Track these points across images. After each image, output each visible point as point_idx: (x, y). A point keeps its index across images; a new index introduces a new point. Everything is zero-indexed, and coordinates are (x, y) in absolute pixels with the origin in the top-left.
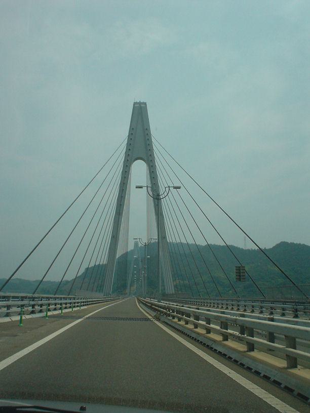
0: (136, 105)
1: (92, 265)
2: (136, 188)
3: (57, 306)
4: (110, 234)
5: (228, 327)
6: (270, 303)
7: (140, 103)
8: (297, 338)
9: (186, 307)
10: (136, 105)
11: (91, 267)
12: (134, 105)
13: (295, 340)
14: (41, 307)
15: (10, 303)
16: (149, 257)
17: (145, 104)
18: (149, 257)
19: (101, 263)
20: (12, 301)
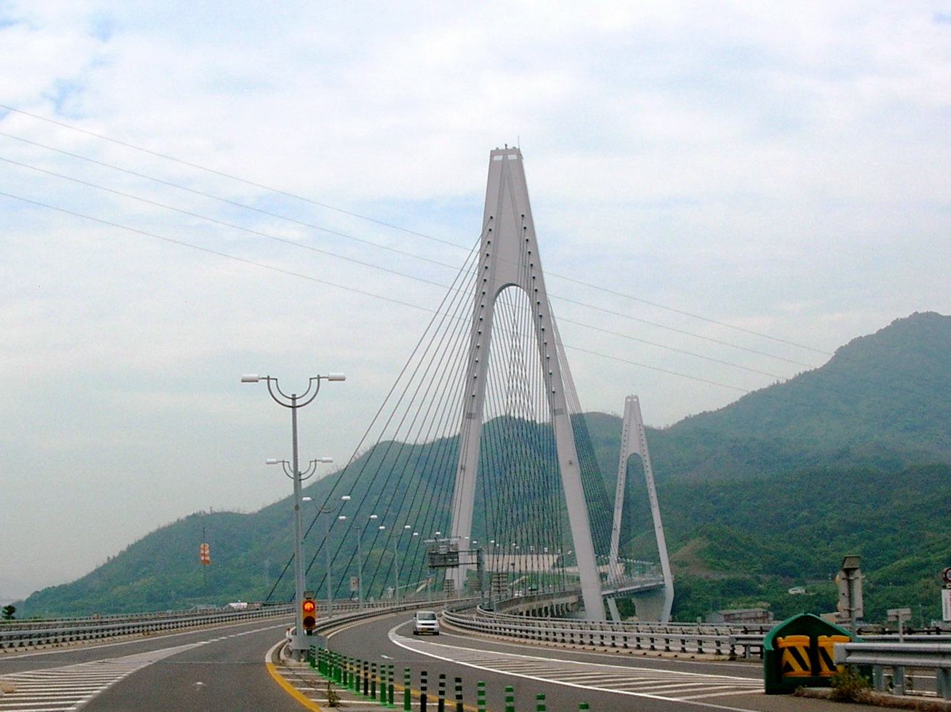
1: (431, 438)
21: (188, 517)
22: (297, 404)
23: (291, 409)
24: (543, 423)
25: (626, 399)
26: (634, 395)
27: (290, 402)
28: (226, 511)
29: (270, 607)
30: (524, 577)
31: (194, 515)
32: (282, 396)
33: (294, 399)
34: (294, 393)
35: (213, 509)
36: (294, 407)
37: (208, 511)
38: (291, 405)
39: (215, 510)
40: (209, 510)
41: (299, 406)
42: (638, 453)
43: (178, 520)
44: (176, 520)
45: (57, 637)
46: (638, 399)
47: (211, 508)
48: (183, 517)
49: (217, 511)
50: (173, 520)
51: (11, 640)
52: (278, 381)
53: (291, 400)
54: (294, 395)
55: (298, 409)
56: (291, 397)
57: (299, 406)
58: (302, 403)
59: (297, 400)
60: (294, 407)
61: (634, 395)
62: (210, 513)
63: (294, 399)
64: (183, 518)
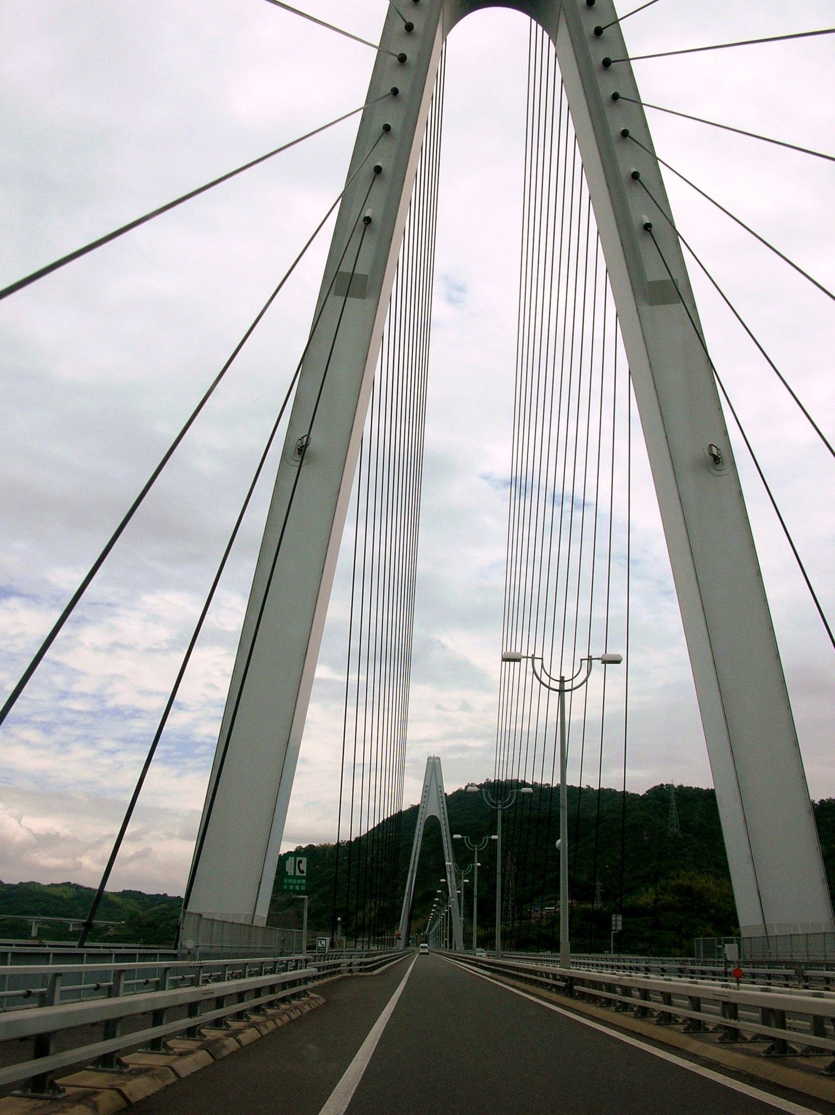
25: (428, 759)
42: (437, 816)
46: (440, 760)
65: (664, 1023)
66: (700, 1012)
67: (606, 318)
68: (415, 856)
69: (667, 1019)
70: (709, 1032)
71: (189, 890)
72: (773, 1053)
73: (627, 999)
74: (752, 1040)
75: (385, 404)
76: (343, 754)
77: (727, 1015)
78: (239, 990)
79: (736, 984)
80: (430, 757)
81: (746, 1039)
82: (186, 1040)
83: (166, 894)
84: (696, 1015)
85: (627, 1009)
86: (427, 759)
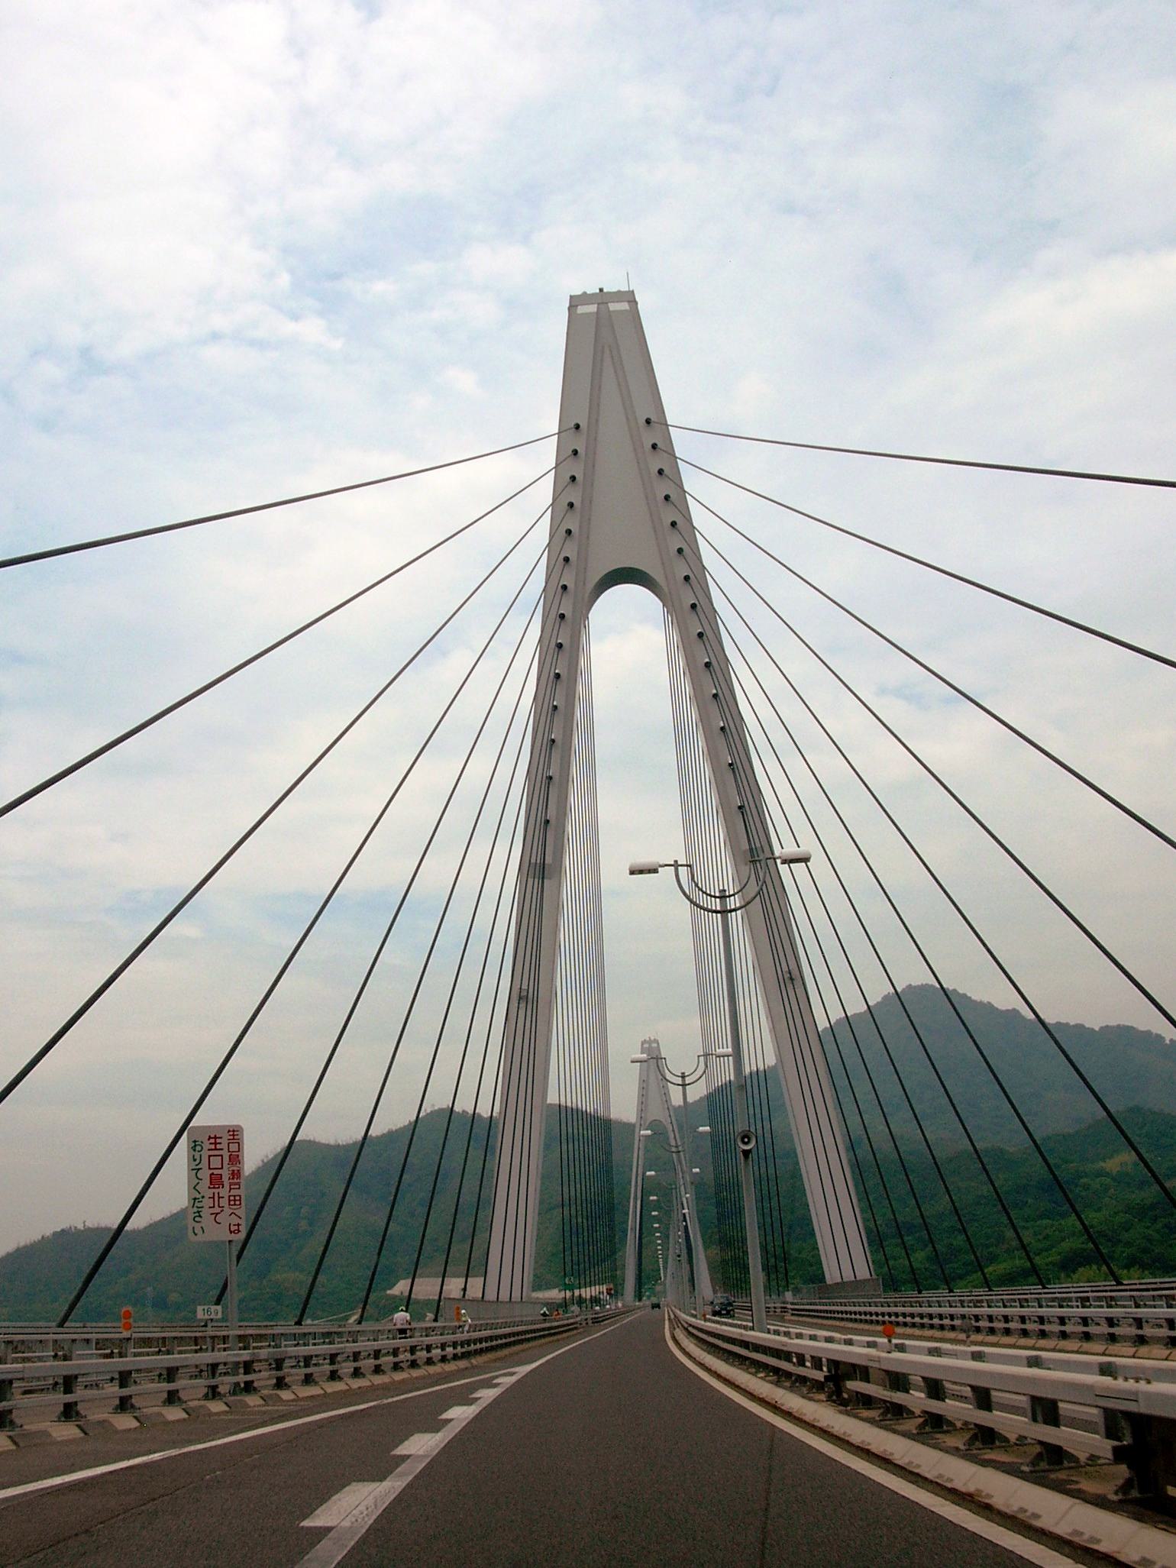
0: (581, 310)
1: (396, 1116)
2: (632, 873)
3: (433, 1351)
4: (499, 984)
5: (993, 1407)
6: (1163, 1303)
7: (602, 297)
8: (1061, 1401)
9: (861, 1344)
10: (581, 310)
11: (391, 1136)
12: (572, 307)
13: (989, 1392)
14: (68, 1390)
15: (128, 1362)
16: (698, 1170)
17: (630, 297)
18: (698, 1170)
19: (439, 1099)
20: (135, 1355)
21: (55, 1234)
22: (687, 1082)
23: (681, 1087)
24: (730, 1081)
25: (642, 1044)
26: (652, 1038)
27: (679, 1081)
28: (103, 1226)
29: (54, 1402)
30: (242, 1410)
31: (63, 1230)
32: (675, 1077)
33: (683, 1076)
34: (683, 1071)
35: (86, 1224)
36: (684, 1085)
37: (81, 1227)
38: (680, 1083)
39: (89, 1224)
40: (83, 1225)
41: (689, 1084)
42: (662, 1120)
43: (43, 1237)
44: (40, 1238)
45: (218, 1380)
46: (658, 1044)
47: (84, 1222)
48: (48, 1233)
49: (91, 1226)
50: (36, 1236)
51: (307, 1365)
52: (667, 1059)
53: (680, 1079)
54: (683, 1073)
55: (687, 1087)
56: (680, 1075)
57: (689, 1084)
58: (692, 1081)
59: (687, 1079)
60: (684, 1085)
61: (652, 1038)
62: (82, 1229)
63: (683, 1076)
64: (48, 1234)
65: (981, 1446)
66: (869, 1382)
67: (835, 678)
68: (637, 1178)
69: (935, 1424)
70: (916, 1417)
71: (73, 1303)
72: (927, 1428)
73: (898, 1397)
74: (1090, 1462)
75: (488, 858)
76: (847, 830)
77: (1040, 1418)
78: (215, 1362)
79: (886, 1340)
80: (645, 1040)
81: (913, 1413)
82: (119, 1413)
83: (910, 985)
84: (983, 1417)
85: (993, 1442)
86: (640, 1044)
